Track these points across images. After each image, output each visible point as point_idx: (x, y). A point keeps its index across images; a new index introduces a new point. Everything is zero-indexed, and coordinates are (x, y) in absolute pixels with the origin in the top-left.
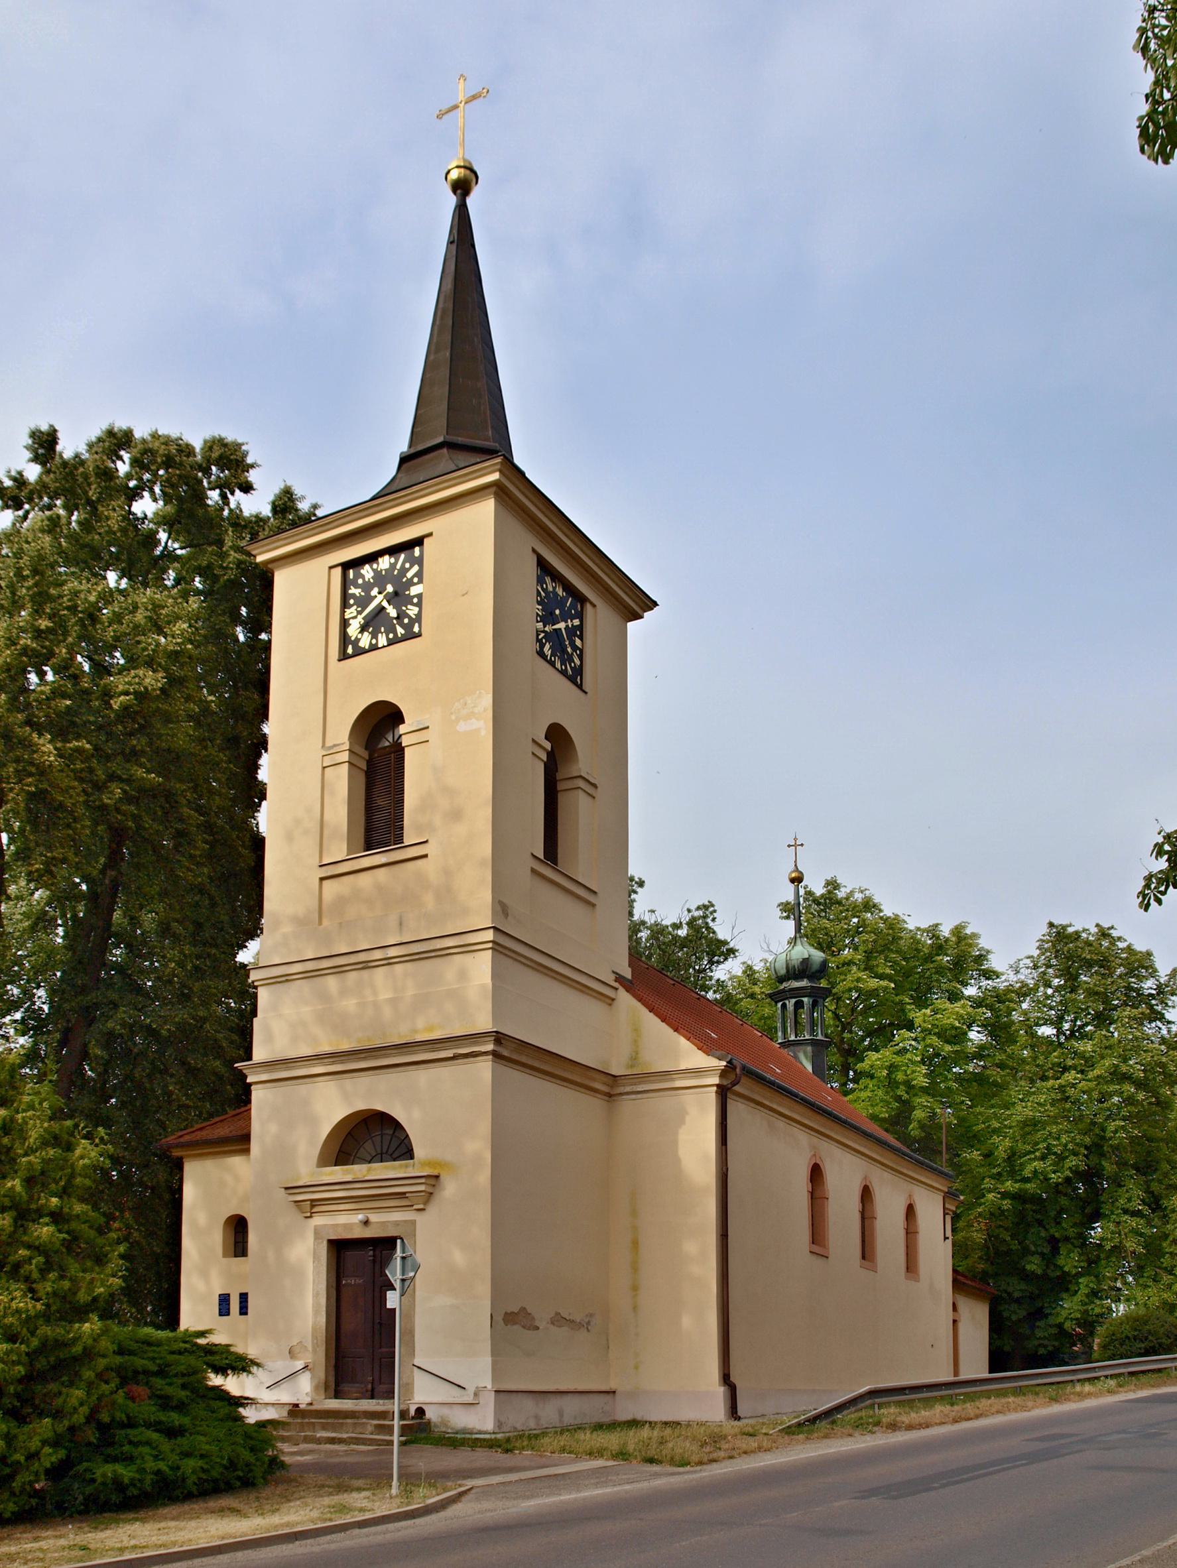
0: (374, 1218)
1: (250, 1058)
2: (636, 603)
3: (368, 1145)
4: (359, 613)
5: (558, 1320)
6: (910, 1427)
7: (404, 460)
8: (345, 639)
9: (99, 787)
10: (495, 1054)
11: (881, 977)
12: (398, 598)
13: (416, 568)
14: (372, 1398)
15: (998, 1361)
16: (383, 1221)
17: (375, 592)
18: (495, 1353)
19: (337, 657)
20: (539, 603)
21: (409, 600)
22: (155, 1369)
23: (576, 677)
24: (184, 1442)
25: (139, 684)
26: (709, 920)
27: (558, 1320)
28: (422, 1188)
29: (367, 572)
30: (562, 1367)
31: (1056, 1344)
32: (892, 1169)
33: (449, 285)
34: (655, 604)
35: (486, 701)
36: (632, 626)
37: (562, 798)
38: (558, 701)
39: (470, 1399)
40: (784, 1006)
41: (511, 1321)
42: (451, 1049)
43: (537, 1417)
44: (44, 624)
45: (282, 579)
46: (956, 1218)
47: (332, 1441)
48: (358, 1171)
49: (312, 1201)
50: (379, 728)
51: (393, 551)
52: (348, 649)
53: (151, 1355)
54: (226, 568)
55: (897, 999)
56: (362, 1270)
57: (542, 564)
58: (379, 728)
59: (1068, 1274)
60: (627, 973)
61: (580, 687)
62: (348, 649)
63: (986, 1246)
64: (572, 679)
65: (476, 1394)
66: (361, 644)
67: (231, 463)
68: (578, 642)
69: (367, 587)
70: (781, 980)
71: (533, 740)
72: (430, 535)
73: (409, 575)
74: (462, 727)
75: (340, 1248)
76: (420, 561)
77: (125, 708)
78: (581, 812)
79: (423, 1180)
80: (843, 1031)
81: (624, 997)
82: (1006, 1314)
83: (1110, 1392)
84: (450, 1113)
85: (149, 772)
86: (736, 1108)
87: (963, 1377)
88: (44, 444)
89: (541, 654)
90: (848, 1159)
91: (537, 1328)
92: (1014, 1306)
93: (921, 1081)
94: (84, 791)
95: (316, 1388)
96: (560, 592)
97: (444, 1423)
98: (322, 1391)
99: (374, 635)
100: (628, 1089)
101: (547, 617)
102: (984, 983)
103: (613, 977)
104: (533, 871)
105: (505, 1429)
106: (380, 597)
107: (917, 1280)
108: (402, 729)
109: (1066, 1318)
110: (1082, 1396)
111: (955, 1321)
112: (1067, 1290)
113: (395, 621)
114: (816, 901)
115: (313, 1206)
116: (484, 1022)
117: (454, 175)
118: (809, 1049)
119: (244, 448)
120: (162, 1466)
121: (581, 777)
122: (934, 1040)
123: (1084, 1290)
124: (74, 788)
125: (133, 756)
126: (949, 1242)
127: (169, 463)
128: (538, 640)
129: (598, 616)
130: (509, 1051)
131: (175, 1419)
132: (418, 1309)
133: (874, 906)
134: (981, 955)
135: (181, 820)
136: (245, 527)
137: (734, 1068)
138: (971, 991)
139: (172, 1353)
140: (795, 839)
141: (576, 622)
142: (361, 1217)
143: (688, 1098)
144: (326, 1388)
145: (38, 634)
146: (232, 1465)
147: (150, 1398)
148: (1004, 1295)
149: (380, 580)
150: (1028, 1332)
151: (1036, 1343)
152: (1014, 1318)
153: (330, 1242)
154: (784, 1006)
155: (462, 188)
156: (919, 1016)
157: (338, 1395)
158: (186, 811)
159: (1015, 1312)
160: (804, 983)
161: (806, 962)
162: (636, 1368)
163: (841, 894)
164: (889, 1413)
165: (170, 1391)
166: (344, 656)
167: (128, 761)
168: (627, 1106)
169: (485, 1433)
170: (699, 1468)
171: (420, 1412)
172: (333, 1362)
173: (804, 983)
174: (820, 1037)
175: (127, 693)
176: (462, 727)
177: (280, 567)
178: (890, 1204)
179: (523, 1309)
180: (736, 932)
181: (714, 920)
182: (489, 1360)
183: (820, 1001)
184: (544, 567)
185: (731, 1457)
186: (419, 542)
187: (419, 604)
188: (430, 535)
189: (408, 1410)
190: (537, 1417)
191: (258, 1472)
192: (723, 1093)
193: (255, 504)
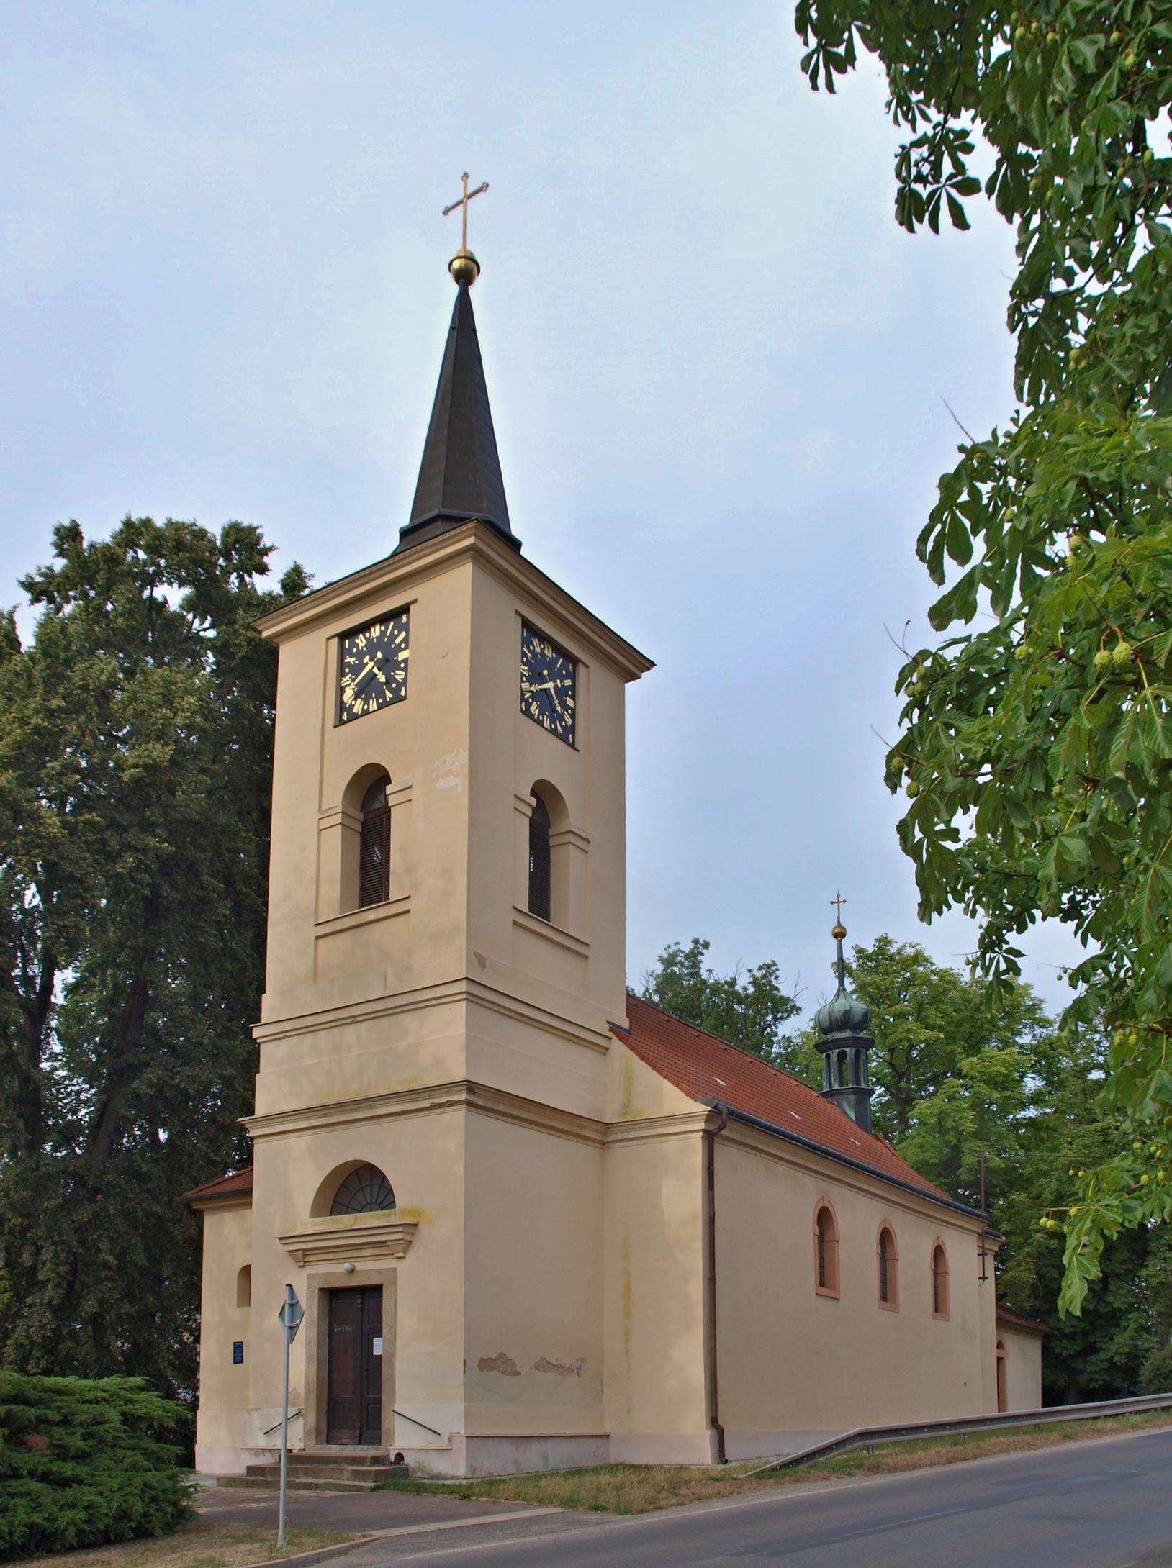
0: (360, 1266)
1: (253, 1114)
2: (631, 663)
3: (359, 1196)
4: (353, 680)
5: (543, 1365)
6: (895, 1469)
7: (404, 533)
8: (341, 706)
9: (114, 857)
10: (468, 1103)
11: (932, 1028)
12: (388, 664)
13: (403, 634)
14: (360, 1443)
15: (1051, 1396)
16: (368, 1269)
17: (366, 659)
18: (467, 1399)
19: (332, 724)
20: (524, 664)
21: (396, 665)
22: (58, 1418)
23: (567, 736)
24: (71, 1493)
25: (148, 756)
26: (772, 979)
27: (543, 1365)
28: (400, 1236)
29: (361, 641)
30: (549, 1412)
31: (1108, 1378)
32: (915, 1211)
33: (450, 369)
34: (653, 664)
35: (462, 759)
36: (630, 687)
37: (555, 855)
38: (544, 758)
39: (443, 1444)
40: (828, 1057)
41: (489, 1367)
42: (423, 1099)
43: (517, 1463)
44: (55, 703)
45: (286, 654)
46: (1000, 1257)
47: (309, 1486)
48: (346, 1221)
49: (304, 1250)
50: (370, 794)
51: (383, 619)
52: (344, 715)
53: (59, 1404)
54: (240, 645)
55: (949, 1048)
56: (353, 1315)
57: (526, 624)
58: (370, 794)
59: (1119, 1309)
60: (625, 1023)
61: (572, 745)
62: (344, 715)
63: (1034, 1287)
64: (563, 738)
65: (450, 1440)
66: (355, 710)
67: (246, 546)
68: (570, 702)
69: (360, 655)
70: (825, 1031)
71: (516, 796)
72: (415, 601)
73: (397, 641)
74: (442, 784)
75: (333, 1296)
76: (406, 628)
77: (137, 781)
78: (570, 867)
79: (400, 1229)
80: (900, 1081)
81: (617, 1046)
82: (1057, 1350)
83: (1135, 1427)
84: (428, 1162)
85: (163, 841)
86: (719, 1150)
87: (1010, 1412)
88: (68, 536)
89: (527, 713)
90: (863, 1202)
91: (519, 1374)
92: (1065, 1342)
93: (969, 1126)
94: (95, 861)
95: (307, 1434)
96: (549, 652)
97: (421, 1469)
98: (314, 1436)
99: (366, 702)
100: (620, 1136)
101: (536, 677)
102: (1038, 1031)
103: (607, 1026)
104: (515, 923)
105: (478, 1474)
106: (371, 664)
107: (947, 1319)
108: (389, 789)
109: (1116, 1353)
110: (1100, 1433)
111: (1000, 1360)
112: (1118, 1326)
113: (383, 689)
114: (869, 958)
115: (305, 1256)
116: (459, 1073)
117: (456, 265)
118: (852, 1097)
119: (259, 531)
120: (37, 1518)
121: (571, 832)
122: (981, 1087)
123: (1133, 1326)
124: (84, 859)
125: (147, 827)
126: (991, 1282)
127: (179, 548)
128: (523, 699)
129: (592, 677)
130: (481, 1099)
131: (68, 1469)
132: (398, 1354)
133: (926, 959)
134: (1034, 1005)
135: (202, 888)
136: (258, 606)
137: (721, 1113)
138: (1025, 1039)
139: (85, 1402)
140: (838, 896)
141: (568, 682)
142: (347, 1266)
143: (670, 1145)
144: (318, 1433)
145: (51, 714)
146: (124, 1515)
147: (48, 1448)
148: (1055, 1332)
149: (372, 647)
150: (1081, 1367)
151: (1087, 1377)
152: (1065, 1353)
153: (321, 1289)
154: (828, 1057)
155: (465, 276)
156: (968, 1063)
157: (329, 1441)
158: (206, 879)
159: (1066, 1349)
160: (847, 1034)
161: (847, 1013)
162: (629, 1411)
163: (893, 949)
164: (888, 1455)
165: (68, 1440)
166: (340, 723)
167: (144, 832)
168: (619, 1153)
169: (457, 1478)
170: (594, 1516)
171: (400, 1457)
172: (325, 1407)
173: (847, 1034)
174: (863, 1086)
175: (136, 766)
176: (442, 784)
177: (284, 641)
178: (914, 1245)
179: (502, 1355)
180: (799, 989)
181: (777, 978)
182: (462, 1405)
183: (863, 1050)
184: (530, 629)
185: (680, 1504)
186: (405, 609)
187: (405, 669)
188: (415, 601)
189: (388, 1455)
190: (517, 1463)
191: (157, 1522)
192: (710, 1137)
193: (268, 584)
